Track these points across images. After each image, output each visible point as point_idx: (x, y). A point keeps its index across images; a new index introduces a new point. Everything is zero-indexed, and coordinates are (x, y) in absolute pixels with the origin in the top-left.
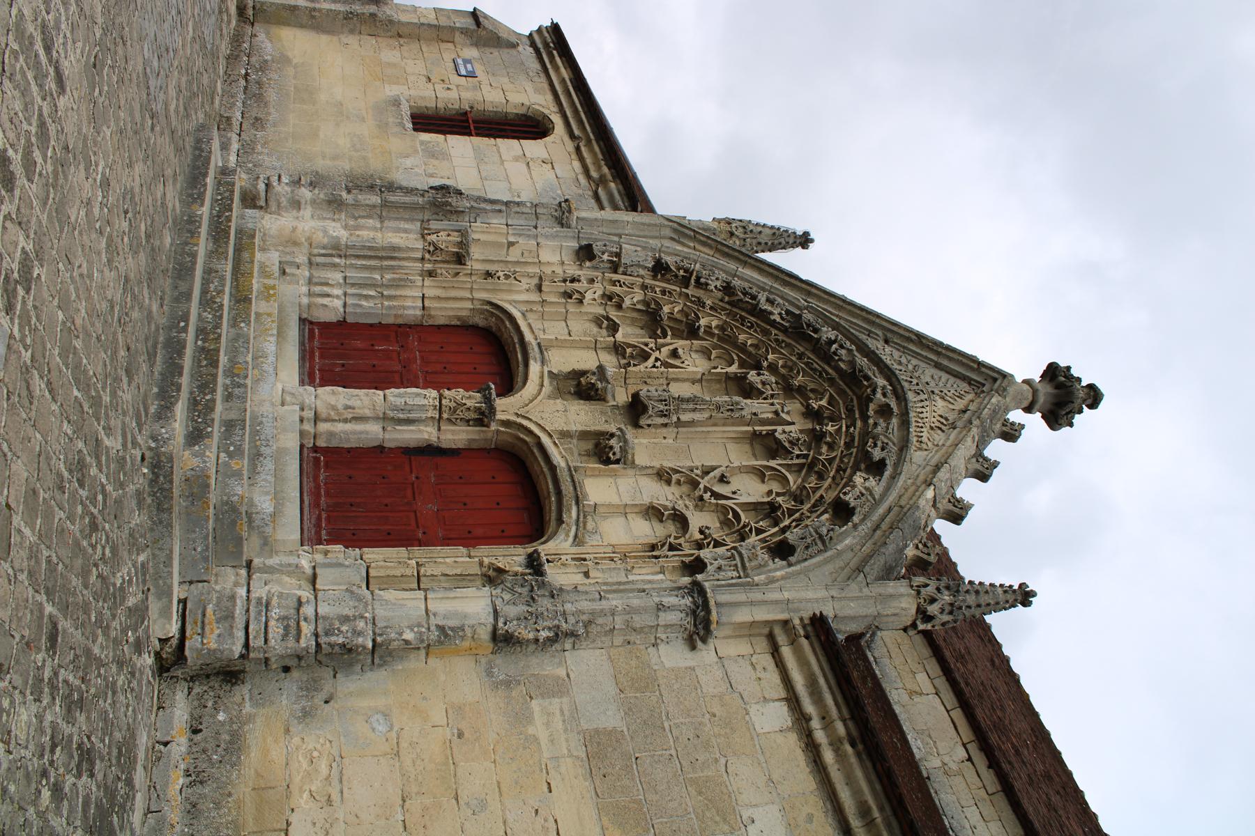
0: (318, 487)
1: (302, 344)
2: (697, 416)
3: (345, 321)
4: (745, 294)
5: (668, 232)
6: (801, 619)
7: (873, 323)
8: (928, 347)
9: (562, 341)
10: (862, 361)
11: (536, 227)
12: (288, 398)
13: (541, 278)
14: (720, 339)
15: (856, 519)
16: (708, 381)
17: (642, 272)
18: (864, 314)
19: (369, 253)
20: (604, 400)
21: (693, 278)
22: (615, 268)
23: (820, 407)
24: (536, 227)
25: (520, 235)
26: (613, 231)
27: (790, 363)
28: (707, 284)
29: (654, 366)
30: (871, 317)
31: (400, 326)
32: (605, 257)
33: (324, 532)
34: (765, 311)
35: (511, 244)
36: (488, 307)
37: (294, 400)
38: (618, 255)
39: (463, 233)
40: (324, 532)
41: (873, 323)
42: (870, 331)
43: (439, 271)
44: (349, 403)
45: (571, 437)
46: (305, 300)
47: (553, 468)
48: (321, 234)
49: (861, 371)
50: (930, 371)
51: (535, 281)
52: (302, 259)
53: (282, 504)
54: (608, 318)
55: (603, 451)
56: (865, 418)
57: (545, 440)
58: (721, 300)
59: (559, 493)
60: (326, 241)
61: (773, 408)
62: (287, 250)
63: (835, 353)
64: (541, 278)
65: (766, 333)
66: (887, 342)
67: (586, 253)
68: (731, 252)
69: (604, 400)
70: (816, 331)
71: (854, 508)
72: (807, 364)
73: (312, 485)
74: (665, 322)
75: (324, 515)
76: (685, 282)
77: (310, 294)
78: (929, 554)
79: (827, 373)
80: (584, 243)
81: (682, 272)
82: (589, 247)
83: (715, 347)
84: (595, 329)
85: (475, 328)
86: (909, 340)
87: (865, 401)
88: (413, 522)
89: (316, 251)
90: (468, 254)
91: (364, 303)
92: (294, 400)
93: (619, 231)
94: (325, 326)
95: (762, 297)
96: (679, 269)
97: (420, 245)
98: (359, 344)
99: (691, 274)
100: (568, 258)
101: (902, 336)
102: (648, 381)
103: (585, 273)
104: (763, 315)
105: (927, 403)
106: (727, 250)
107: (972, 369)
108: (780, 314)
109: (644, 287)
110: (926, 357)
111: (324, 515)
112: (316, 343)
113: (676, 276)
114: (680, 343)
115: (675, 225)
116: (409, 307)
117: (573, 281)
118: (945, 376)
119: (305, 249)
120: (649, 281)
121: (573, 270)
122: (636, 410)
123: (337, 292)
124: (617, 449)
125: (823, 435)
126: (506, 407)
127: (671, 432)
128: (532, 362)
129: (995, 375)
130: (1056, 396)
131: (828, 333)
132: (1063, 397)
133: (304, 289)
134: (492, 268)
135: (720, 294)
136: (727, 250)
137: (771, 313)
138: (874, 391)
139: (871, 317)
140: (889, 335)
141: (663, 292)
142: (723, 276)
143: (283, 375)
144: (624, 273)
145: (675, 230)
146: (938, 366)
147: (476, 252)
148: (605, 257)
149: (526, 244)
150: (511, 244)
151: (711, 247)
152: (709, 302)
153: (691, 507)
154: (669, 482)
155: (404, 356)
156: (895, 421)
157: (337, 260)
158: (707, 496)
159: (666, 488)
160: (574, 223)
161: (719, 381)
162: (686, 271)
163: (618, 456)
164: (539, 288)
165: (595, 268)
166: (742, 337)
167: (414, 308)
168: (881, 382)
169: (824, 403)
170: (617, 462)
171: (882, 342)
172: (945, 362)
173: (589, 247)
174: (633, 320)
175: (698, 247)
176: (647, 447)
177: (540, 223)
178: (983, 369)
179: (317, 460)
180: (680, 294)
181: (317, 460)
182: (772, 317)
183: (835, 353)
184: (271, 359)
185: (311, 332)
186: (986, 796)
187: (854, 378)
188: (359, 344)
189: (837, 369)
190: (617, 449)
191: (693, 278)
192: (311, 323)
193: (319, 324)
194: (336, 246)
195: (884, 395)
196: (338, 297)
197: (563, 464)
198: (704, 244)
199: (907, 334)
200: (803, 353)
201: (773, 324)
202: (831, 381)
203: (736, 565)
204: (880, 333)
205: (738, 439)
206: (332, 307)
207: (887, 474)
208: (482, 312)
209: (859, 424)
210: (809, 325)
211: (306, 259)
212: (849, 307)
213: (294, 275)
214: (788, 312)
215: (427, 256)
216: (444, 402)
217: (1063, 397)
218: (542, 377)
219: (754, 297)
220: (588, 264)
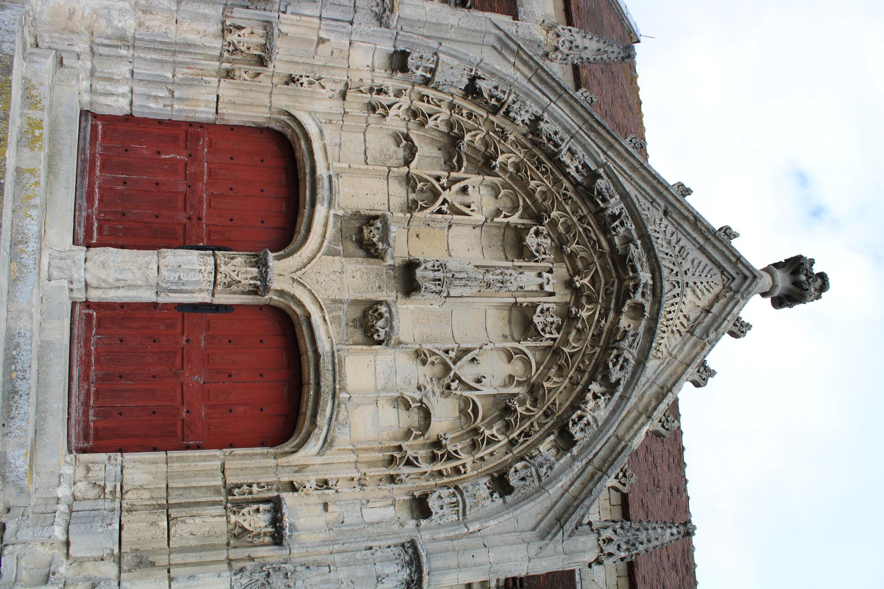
0: (88, 354)
1: (81, 151)
2: (467, 291)
3: (131, 114)
4: (549, 139)
5: (491, 40)
6: (498, 580)
7: (659, 193)
8: (701, 230)
9: (353, 169)
10: (637, 251)
11: (351, 23)
12: (55, 273)
13: (347, 84)
14: (511, 177)
15: (575, 450)
16: (488, 227)
17: (453, 90)
18: (655, 182)
19: (161, 47)
20: (383, 259)
21: (504, 110)
22: (426, 82)
23: (582, 285)
24: (351, 23)
25: (333, 31)
26: (434, 34)
27: (570, 222)
28: (515, 119)
29: (440, 212)
30: (660, 187)
31: (191, 124)
32: (419, 72)
33: (91, 412)
34: (563, 162)
35: (321, 41)
36: (284, 118)
37: (61, 275)
38: (433, 71)
39: (268, 25)
40: (91, 412)
41: (659, 193)
42: (654, 200)
43: (237, 73)
44: (120, 277)
45: (343, 303)
46: (86, 98)
47: (317, 355)
48: (103, 23)
49: (631, 261)
50: (695, 254)
51: (341, 87)
52: (82, 46)
53: (45, 419)
54: (407, 137)
55: (370, 323)
56: (618, 312)
57: (316, 318)
58: (524, 135)
59: (318, 384)
60: (109, 32)
61: (540, 280)
62: (64, 36)
63: (614, 229)
64: (347, 84)
65: (556, 182)
66: (666, 213)
67: (399, 61)
68: (549, 81)
69: (383, 259)
70: (604, 200)
71: (577, 441)
72: (585, 230)
73: (83, 351)
74: (464, 148)
75: (93, 389)
76: (495, 111)
77: (92, 91)
78: (624, 485)
79: (600, 247)
80: (401, 48)
81: (493, 102)
82: (404, 55)
83: (505, 186)
84: (393, 147)
85: (270, 130)
86: (686, 218)
87: (624, 295)
88: (179, 397)
89: (98, 40)
90: (271, 60)
91: (152, 105)
92: (61, 275)
93: (441, 35)
94: (110, 121)
95: (564, 148)
96: (492, 97)
97: (218, 44)
98: (145, 150)
99: (502, 105)
100: (381, 60)
101: (681, 213)
102: (431, 224)
103: (392, 83)
104: (561, 166)
105: (678, 299)
106: (546, 77)
107: (730, 261)
108: (577, 168)
109: (452, 106)
110: (694, 239)
111: (93, 389)
112: (98, 149)
113: (487, 103)
114: (474, 180)
115: (502, 34)
116: (201, 112)
117: (380, 91)
118: (705, 260)
119: (86, 37)
120: (458, 101)
121: (382, 78)
122: (408, 279)
123: (124, 89)
124: (382, 333)
125: (576, 318)
126: (282, 271)
127: (439, 299)
128: (319, 207)
129: (747, 273)
130: (790, 290)
131: (615, 206)
132: (798, 282)
133: (85, 84)
134: (296, 72)
135: (525, 129)
136: (546, 77)
137: (568, 166)
138: (636, 287)
139: (660, 187)
140: (670, 209)
141: (470, 115)
142: (535, 109)
143: (52, 235)
144: (435, 89)
145: (499, 39)
146: (701, 249)
147: (281, 47)
148: (419, 72)
149: (338, 41)
150: (321, 41)
151: (531, 68)
152: (511, 137)
153: (438, 394)
154: (424, 363)
155: (191, 169)
156: (644, 323)
157: (123, 52)
158: (454, 385)
159: (420, 367)
160: (393, 24)
161: (499, 227)
162: (498, 100)
163: (382, 338)
164: (344, 96)
165: (405, 80)
166: (533, 184)
167: (207, 112)
168: (645, 276)
169: (586, 281)
170: (380, 343)
171: (661, 213)
172: (709, 249)
173: (404, 55)
174: (433, 141)
175: (519, 64)
176: (410, 318)
177: (358, 18)
178: (740, 265)
179: (89, 317)
180: (487, 119)
181: (89, 317)
182: (568, 170)
183: (614, 229)
184: (33, 245)
185: (94, 128)
186: (608, 506)
187: (621, 261)
188: (145, 150)
189: (611, 242)
190: (382, 333)
191: (504, 110)
192: (95, 116)
193: (102, 117)
194: (123, 38)
195: (643, 294)
196: (123, 95)
197: (328, 348)
198: (525, 63)
199: (686, 213)
200: (585, 217)
201: (567, 175)
202: (602, 255)
203: (458, 511)
204: (663, 204)
205: (500, 307)
206: (118, 106)
207: (617, 395)
208: (279, 121)
209: (611, 315)
210: (600, 193)
211: (87, 47)
212: (644, 172)
213: (72, 67)
214: (585, 165)
215: (226, 54)
216: (219, 276)
217: (798, 282)
218: (327, 218)
219: (556, 145)
220: (399, 75)
